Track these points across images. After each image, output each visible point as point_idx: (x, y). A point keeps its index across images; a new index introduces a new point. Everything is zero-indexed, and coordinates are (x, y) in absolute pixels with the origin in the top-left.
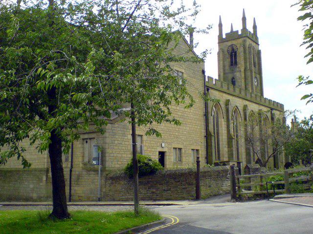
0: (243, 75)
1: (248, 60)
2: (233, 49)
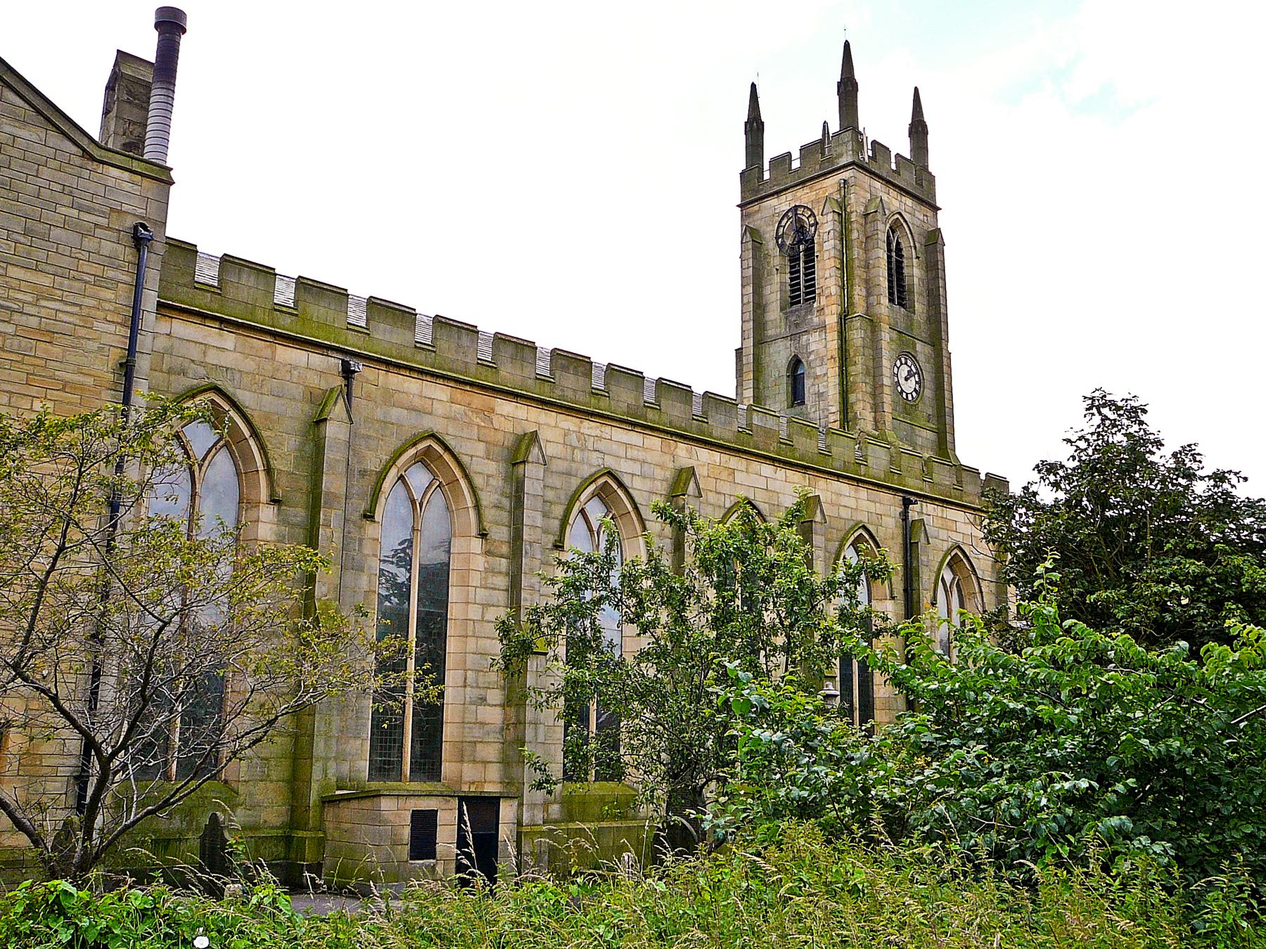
0: (834, 345)
1: (859, 272)
2: (800, 229)
